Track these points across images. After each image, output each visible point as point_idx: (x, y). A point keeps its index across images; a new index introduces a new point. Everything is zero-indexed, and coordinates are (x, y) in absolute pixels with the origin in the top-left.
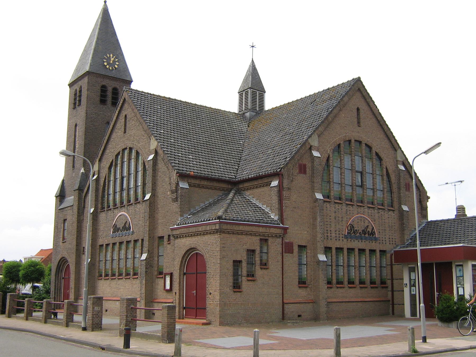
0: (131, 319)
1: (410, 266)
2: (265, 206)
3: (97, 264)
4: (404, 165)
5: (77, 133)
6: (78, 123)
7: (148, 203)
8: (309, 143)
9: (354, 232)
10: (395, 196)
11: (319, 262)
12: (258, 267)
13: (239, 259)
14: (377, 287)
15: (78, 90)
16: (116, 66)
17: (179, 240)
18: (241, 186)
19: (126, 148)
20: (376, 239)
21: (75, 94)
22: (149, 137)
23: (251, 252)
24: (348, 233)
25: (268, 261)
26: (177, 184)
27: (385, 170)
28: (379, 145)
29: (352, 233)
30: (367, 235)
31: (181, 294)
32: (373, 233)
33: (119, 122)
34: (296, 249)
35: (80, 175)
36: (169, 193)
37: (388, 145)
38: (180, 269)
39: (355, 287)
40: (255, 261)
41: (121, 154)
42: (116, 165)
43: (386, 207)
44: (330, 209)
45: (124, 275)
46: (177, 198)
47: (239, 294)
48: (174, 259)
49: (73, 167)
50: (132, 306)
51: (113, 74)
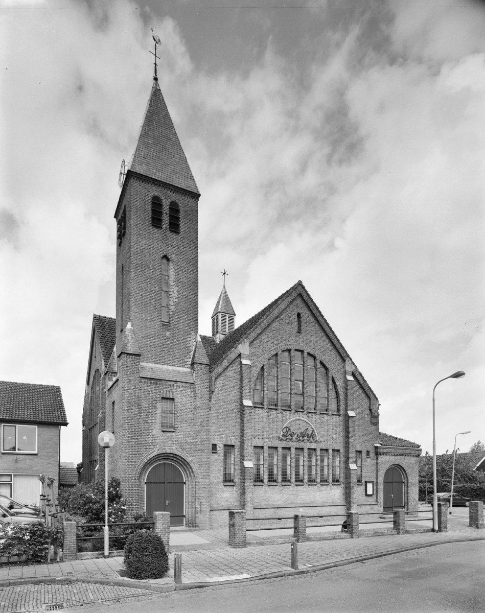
5: (289, 383)
17: (383, 456)
24: (283, 435)
30: (306, 438)
32: (313, 436)
43: (265, 407)
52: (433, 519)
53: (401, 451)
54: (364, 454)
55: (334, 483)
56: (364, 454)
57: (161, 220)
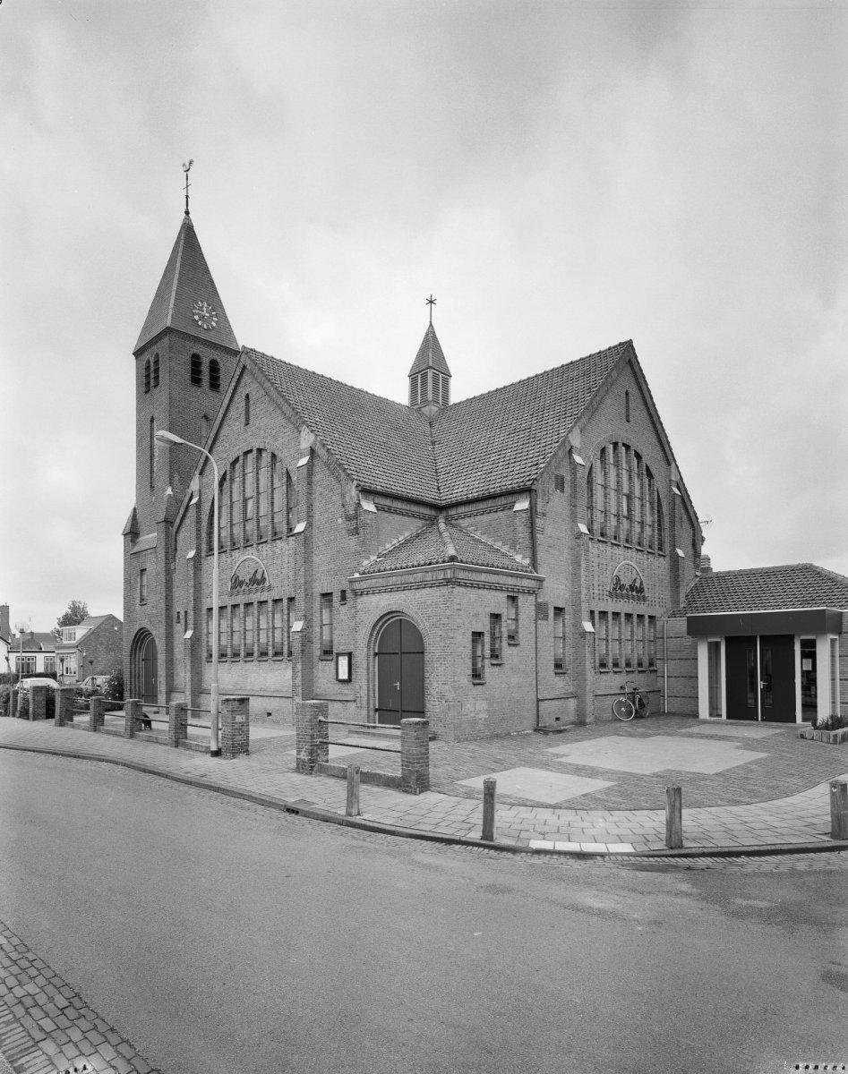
0: (321, 742)
1: (710, 640)
2: (500, 544)
3: (204, 637)
4: (678, 488)
6: (156, 415)
7: (301, 537)
8: (569, 442)
9: (620, 588)
10: (666, 533)
11: (584, 634)
12: (505, 644)
13: (479, 630)
14: (645, 671)
15: (152, 360)
16: (214, 324)
17: (365, 598)
18: (452, 512)
19: (251, 451)
20: (644, 599)
21: (148, 368)
22: (297, 428)
23: (496, 617)
25: (517, 632)
26: (359, 504)
27: (656, 493)
28: (651, 456)
29: (618, 590)
31: (371, 687)
32: (641, 590)
33: (233, 408)
34: (551, 612)
35: (166, 499)
36: (340, 521)
37: (660, 456)
38: (368, 647)
39: (620, 672)
40: (501, 632)
41: (241, 461)
42: (232, 480)
44: (594, 548)
45: (256, 655)
46: (357, 528)
47: (480, 687)
48: (355, 629)
49: (152, 487)
50: (322, 718)
51: (211, 337)
52: (487, 841)
53: (399, 578)
54: (336, 598)
55: (275, 658)
56: (336, 598)
57: (201, 380)
